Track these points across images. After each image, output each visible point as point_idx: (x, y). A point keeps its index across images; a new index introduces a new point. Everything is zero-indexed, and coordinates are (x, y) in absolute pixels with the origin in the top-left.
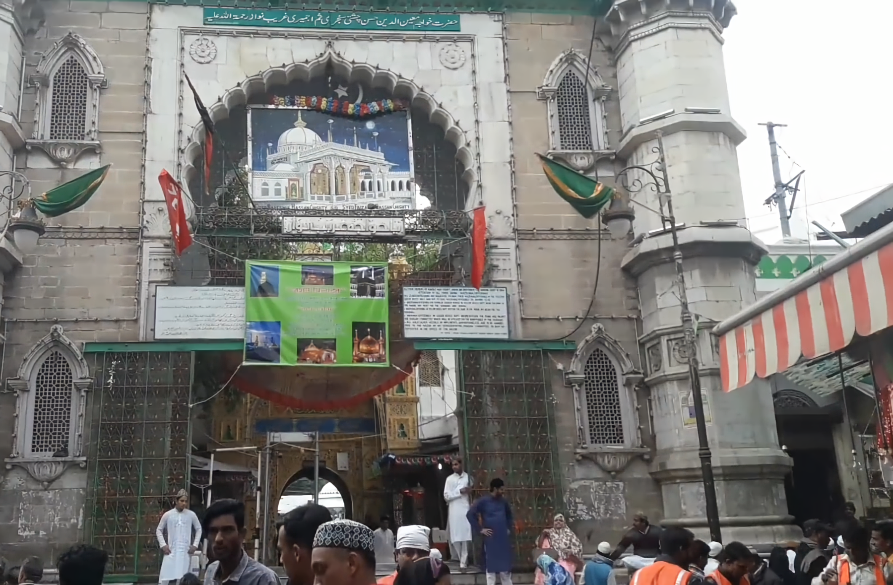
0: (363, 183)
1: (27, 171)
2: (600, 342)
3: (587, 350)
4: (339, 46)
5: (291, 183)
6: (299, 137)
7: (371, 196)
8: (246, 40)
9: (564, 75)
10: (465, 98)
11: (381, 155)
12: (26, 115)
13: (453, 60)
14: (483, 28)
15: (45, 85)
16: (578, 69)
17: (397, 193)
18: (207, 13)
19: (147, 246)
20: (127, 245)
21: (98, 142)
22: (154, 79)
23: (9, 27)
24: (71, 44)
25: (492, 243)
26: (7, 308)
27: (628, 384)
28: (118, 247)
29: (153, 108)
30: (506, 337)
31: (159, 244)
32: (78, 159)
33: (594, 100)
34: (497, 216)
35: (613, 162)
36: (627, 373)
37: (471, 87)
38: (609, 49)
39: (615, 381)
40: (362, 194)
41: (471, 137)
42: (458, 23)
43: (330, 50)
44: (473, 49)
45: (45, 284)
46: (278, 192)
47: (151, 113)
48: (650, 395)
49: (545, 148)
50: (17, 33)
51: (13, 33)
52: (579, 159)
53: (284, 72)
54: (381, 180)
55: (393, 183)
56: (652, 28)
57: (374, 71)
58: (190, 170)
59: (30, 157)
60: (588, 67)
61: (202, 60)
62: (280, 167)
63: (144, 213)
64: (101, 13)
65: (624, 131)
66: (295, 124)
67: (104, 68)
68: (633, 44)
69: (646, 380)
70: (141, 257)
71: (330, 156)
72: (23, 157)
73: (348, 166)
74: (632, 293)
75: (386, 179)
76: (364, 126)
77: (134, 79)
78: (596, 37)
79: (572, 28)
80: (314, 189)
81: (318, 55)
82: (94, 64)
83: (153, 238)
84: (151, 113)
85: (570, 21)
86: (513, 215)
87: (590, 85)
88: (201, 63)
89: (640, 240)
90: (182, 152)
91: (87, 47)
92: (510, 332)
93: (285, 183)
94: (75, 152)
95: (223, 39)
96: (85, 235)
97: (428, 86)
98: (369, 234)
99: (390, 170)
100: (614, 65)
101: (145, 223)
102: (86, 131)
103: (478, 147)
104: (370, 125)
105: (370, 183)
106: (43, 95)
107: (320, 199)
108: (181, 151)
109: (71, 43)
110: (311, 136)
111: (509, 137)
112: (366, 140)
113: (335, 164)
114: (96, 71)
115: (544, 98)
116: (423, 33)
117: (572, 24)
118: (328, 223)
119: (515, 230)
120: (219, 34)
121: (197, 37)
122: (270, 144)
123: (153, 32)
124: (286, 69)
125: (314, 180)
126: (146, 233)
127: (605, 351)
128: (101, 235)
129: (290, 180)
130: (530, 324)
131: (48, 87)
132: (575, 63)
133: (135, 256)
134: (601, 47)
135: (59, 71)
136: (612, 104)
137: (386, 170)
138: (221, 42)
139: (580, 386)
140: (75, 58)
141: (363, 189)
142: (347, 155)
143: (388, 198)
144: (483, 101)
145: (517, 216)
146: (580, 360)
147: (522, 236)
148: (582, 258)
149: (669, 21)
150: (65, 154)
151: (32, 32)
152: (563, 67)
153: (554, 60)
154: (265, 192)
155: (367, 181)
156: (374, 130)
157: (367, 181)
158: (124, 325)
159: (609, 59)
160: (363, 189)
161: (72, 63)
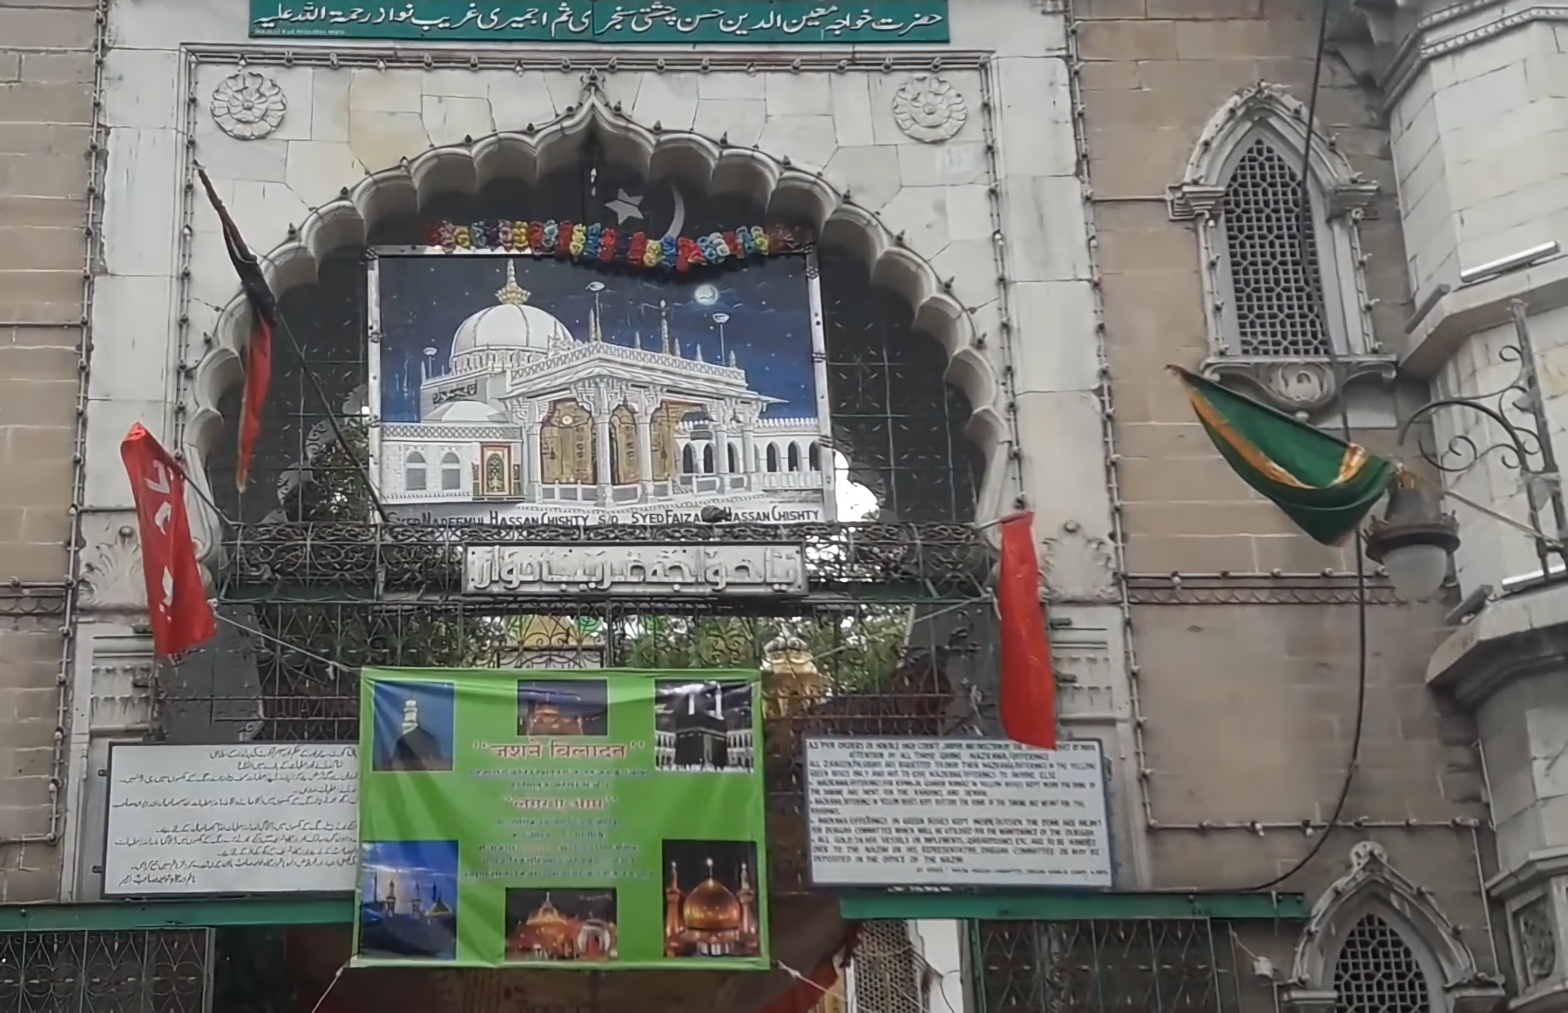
0: (688, 451)
2: (1375, 896)
4: (619, 88)
5: (489, 453)
6: (510, 331)
7: (710, 486)
9: (1242, 152)
10: (969, 217)
11: (736, 376)
17: (783, 478)
19: (88, 635)
20: (33, 631)
22: (113, 183)
25: (1057, 613)
29: (111, 260)
30: (1105, 881)
31: (120, 628)
33: (1329, 221)
34: (1068, 540)
38: (1367, 82)
40: (687, 481)
41: (987, 323)
42: (945, 20)
43: (593, 99)
46: (452, 480)
47: (104, 271)
52: (1293, 381)
54: (737, 443)
55: (771, 449)
60: (1310, 131)
61: (246, 131)
62: (458, 412)
63: (81, 543)
65: (1419, 303)
68: (1434, 67)
70: (71, 664)
71: (594, 380)
73: (645, 404)
74: (1462, 755)
76: (690, 297)
80: (554, 467)
81: (562, 111)
84: (104, 271)
86: (1112, 536)
92: (1115, 866)
93: (470, 455)
97: (861, 189)
98: (708, 590)
99: (762, 415)
100: (1384, 124)
101: (83, 570)
103: (1006, 348)
104: (705, 295)
105: (708, 449)
107: (569, 495)
110: (543, 326)
111: (1091, 322)
112: (698, 337)
113: (609, 400)
116: (849, 48)
117: (1260, 17)
119: (1120, 578)
120: (290, 62)
122: (431, 351)
123: (111, 58)
125: (553, 444)
126: (84, 599)
127: (1393, 924)
129: (484, 446)
130: (1172, 843)
132: (1273, 121)
134: (1344, 77)
136: (1383, 229)
137: (750, 414)
138: (299, 84)
141: (689, 466)
142: (644, 377)
143: (756, 491)
144: (1017, 226)
145: (1124, 537)
147: (1141, 595)
153: (1215, 106)
154: (417, 480)
155: (699, 447)
156: (717, 309)
157: (699, 447)
158: (20, 856)
159: (1369, 108)
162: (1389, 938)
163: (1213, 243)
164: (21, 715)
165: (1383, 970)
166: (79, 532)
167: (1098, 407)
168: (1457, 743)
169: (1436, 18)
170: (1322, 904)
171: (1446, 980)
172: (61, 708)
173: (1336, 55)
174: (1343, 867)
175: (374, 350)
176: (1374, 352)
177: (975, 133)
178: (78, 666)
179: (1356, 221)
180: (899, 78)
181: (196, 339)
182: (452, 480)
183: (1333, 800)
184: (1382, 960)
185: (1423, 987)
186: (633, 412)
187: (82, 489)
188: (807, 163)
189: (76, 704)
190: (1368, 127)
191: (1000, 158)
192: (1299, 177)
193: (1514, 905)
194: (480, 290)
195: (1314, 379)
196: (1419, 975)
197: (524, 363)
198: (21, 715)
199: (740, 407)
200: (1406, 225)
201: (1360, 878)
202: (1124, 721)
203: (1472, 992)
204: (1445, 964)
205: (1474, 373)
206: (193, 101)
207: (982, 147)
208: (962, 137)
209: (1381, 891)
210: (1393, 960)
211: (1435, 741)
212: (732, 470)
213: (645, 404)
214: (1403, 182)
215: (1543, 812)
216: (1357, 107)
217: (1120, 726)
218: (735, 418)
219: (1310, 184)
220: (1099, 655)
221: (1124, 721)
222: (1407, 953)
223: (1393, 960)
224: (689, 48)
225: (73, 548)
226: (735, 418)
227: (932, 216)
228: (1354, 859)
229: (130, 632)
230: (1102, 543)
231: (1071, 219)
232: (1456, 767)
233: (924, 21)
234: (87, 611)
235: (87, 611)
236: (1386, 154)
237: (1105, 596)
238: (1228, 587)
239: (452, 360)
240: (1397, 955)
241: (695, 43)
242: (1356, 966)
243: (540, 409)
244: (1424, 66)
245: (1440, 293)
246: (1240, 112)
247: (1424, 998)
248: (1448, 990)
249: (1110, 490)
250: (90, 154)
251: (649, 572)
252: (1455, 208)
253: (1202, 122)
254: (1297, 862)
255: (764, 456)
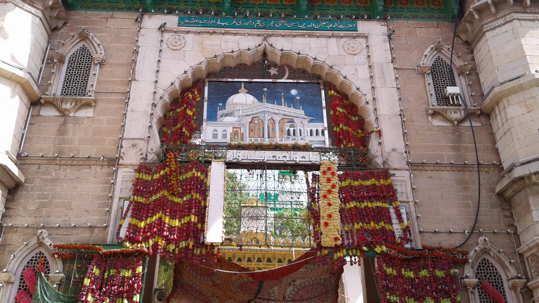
0: (289, 130)
1: (39, 118)
2: (486, 252)
3: (477, 259)
4: (272, 40)
5: (235, 130)
6: (242, 99)
7: (295, 139)
8: (207, 36)
9: (435, 59)
10: (364, 73)
11: (302, 112)
12: (44, 82)
13: (353, 49)
14: (374, 30)
15: (62, 61)
16: (445, 55)
18: (181, 19)
19: (121, 172)
20: (106, 170)
21: (93, 98)
22: (139, 58)
23: (38, 19)
24: (84, 37)
26: (6, 216)
27: (514, 288)
28: (101, 172)
29: (136, 77)
32: (79, 109)
33: (459, 76)
34: (393, 153)
35: (479, 116)
36: (512, 279)
37: (367, 66)
38: (467, 43)
39: (502, 286)
40: (288, 138)
41: (369, 98)
42: (356, 26)
43: (265, 43)
44: (367, 42)
45: (39, 199)
46: (225, 136)
47: (135, 80)
48: (533, 296)
49: (426, 106)
50: (43, 23)
51: (41, 22)
52: (453, 113)
53: (232, 57)
54: (302, 129)
55: (311, 131)
56: (501, 21)
57: (297, 55)
58: (160, 119)
59: (43, 108)
60: (452, 53)
61: (175, 48)
62: (228, 119)
63: (122, 147)
64: (107, 19)
65: (485, 94)
66: (239, 91)
67: (105, 51)
68: (487, 34)
69: (529, 284)
70: (116, 179)
71: (264, 112)
72: (37, 108)
73: (277, 118)
74: (507, 213)
75: (306, 128)
76: (289, 93)
77: (125, 58)
78: (456, 35)
79: (438, 29)
80: (252, 133)
81: (257, 45)
82: (98, 49)
83: (126, 166)
84: (135, 80)
85: (436, 25)
86: (406, 152)
87: (455, 65)
88: (174, 50)
89: (510, 170)
90: (155, 106)
91: (95, 39)
93: (230, 130)
94: (76, 105)
95: (191, 36)
96: (75, 163)
97: (335, 65)
98: (294, 162)
99: (309, 122)
100: (472, 52)
101: (122, 154)
102: (87, 91)
103: (375, 104)
104: (294, 92)
105: (294, 130)
106: (59, 69)
108: (154, 105)
109: (84, 37)
110: (250, 98)
111: (397, 98)
112: (291, 101)
113: (268, 117)
114: (99, 54)
115: (423, 74)
116: (331, 32)
117: (438, 27)
118: (261, 155)
119: (408, 163)
120: (188, 32)
121: (173, 34)
122: (221, 104)
123: (142, 30)
124: (234, 53)
125: (252, 128)
126: (121, 162)
127: (491, 260)
128: (87, 163)
129: (234, 128)
130: (427, 236)
131: (64, 63)
132: (442, 51)
133: (110, 178)
134: (460, 41)
135: (74, 54)
136: (473, 77)
137: (306, 122)
138: (190, 38)
139: (473, 288)
140: (86, 46)
141: (289, 134)
142: (277, 112)
144: (377, 73)
145: (409, 152)
146: (472, 267)
147: (415, 168)
148: (464, 185)
149: (515, 16)
150: (68, 106)
151: (56, 29)
152: (434, 54)
153: (427, 48)
155: (292, 130)
156: (297, 96)
157: (292, 130)
159: (467, 49)
160: (289, 134)
161: (84, 49)
162: (490, 265)
163: (429, 79)
164: (101, 192)
165: (489, 274)
166: (121, 145)
167: (400, 119)
168: (506, 209)
169: (487, 21)
170: (472, 253)
171: (508, 277)
172: (112, 190)
173: (458, 36)
174: (476, 244)
175: (206, 104)
176: (474, 106)
177: (365, 52)
178: (118, 179)
179: (466, 74)
180: (344, 40)
181: (158, 96)
182: (225, 136)
183: (472, 225)
184: (489, 271)
185: (501, 279)
186: (274, 120)
187: (123, 133)
188: (321, 58)
189: (116, 189)
190: (467, 53)
191: (371, 58)
192: (450, 64)
193: (527, 255)
194: (234, 89)
195: (458, 112)
196: (500, 276)
197: (245, 108)
198: (101, 192)
199: (303, 120)
200: (480, 76)
201: (482, 247)
202: (412, 202)
203: (517, 280)
204: (507, 272)
205: (505, 107)
206: (162, 41)
207: (366, 56)
208: (361, 53)
209: (487, 250)
210: (492, 271)
211: (499, 209)
212: (300, 135)
213: (277, 118)
214: (478, 65)
215: (537, 226)
216: (464, 48)
217: (410, 203)
218: (301, 122)
219: (453, 67)
220: (404, 183)
221: (412, 202)
222: (496, 270)
223: (492, 271)
224: (290, 31)
225: (119, 148)
226: (301, 122)
227: (353, 72)
228: (479, 241)
229: (133, 171)
230: (403, 154)
231: (391, 74)
232: (506, 216)
233: (351, 26)
234: (121, 165)
235: (121, 165)
236: (473, 59)
237: (404, 168)
238: (438, 165)
239: (226, 106)
240: (493, 270)
241: (292, 30)
242: (481, 273)
243: (249, 119)
244: (484, 34)
245: (493, 88)
246: (434, 48)
247: (502, 282)
248: (509, 280)
249: (404, 140)
250: (134, 52)
251: (277, 157)
252: (496, 66)
253: (424, 51)
254: (462, 242)
255: (309, 132)
